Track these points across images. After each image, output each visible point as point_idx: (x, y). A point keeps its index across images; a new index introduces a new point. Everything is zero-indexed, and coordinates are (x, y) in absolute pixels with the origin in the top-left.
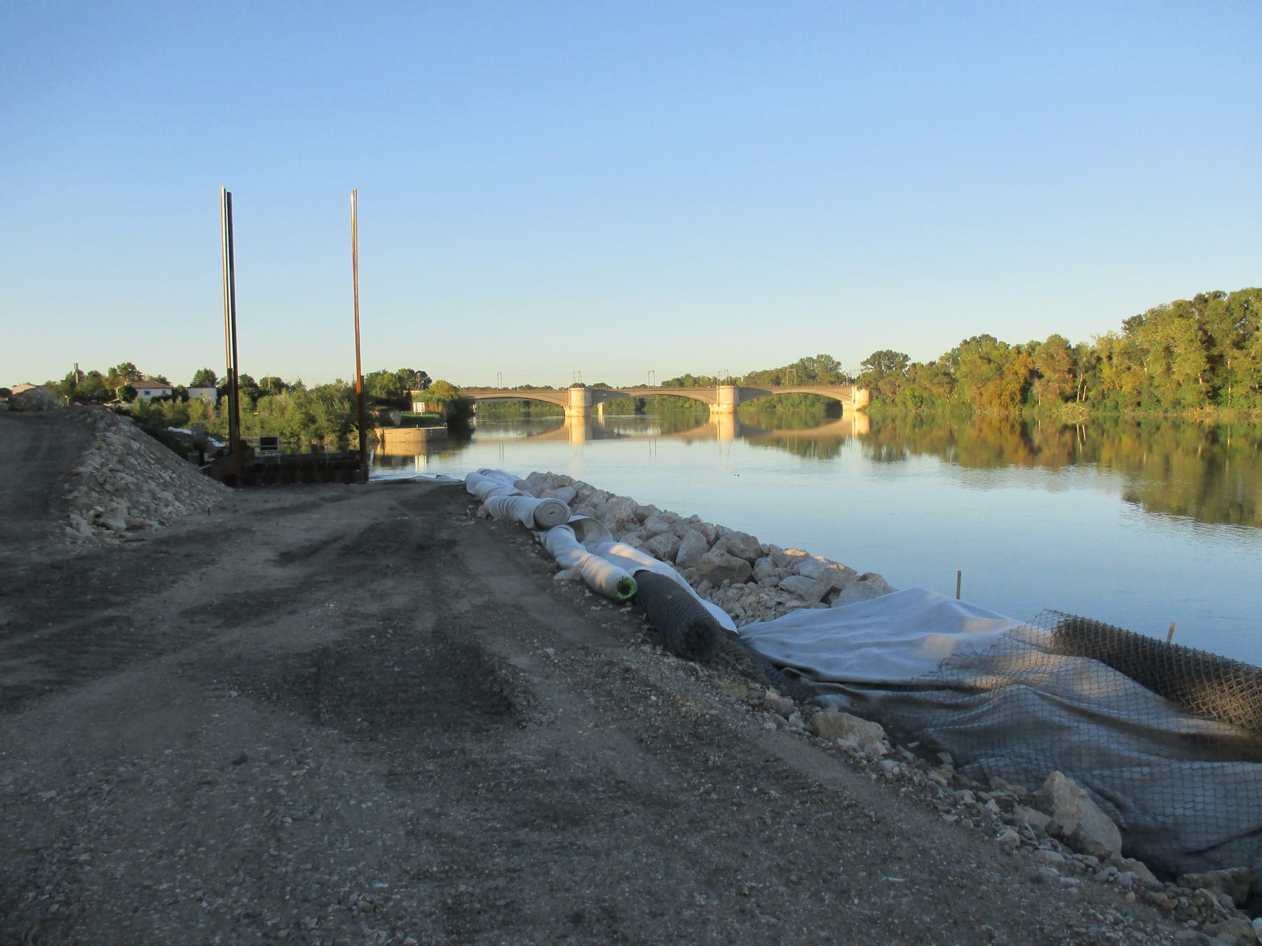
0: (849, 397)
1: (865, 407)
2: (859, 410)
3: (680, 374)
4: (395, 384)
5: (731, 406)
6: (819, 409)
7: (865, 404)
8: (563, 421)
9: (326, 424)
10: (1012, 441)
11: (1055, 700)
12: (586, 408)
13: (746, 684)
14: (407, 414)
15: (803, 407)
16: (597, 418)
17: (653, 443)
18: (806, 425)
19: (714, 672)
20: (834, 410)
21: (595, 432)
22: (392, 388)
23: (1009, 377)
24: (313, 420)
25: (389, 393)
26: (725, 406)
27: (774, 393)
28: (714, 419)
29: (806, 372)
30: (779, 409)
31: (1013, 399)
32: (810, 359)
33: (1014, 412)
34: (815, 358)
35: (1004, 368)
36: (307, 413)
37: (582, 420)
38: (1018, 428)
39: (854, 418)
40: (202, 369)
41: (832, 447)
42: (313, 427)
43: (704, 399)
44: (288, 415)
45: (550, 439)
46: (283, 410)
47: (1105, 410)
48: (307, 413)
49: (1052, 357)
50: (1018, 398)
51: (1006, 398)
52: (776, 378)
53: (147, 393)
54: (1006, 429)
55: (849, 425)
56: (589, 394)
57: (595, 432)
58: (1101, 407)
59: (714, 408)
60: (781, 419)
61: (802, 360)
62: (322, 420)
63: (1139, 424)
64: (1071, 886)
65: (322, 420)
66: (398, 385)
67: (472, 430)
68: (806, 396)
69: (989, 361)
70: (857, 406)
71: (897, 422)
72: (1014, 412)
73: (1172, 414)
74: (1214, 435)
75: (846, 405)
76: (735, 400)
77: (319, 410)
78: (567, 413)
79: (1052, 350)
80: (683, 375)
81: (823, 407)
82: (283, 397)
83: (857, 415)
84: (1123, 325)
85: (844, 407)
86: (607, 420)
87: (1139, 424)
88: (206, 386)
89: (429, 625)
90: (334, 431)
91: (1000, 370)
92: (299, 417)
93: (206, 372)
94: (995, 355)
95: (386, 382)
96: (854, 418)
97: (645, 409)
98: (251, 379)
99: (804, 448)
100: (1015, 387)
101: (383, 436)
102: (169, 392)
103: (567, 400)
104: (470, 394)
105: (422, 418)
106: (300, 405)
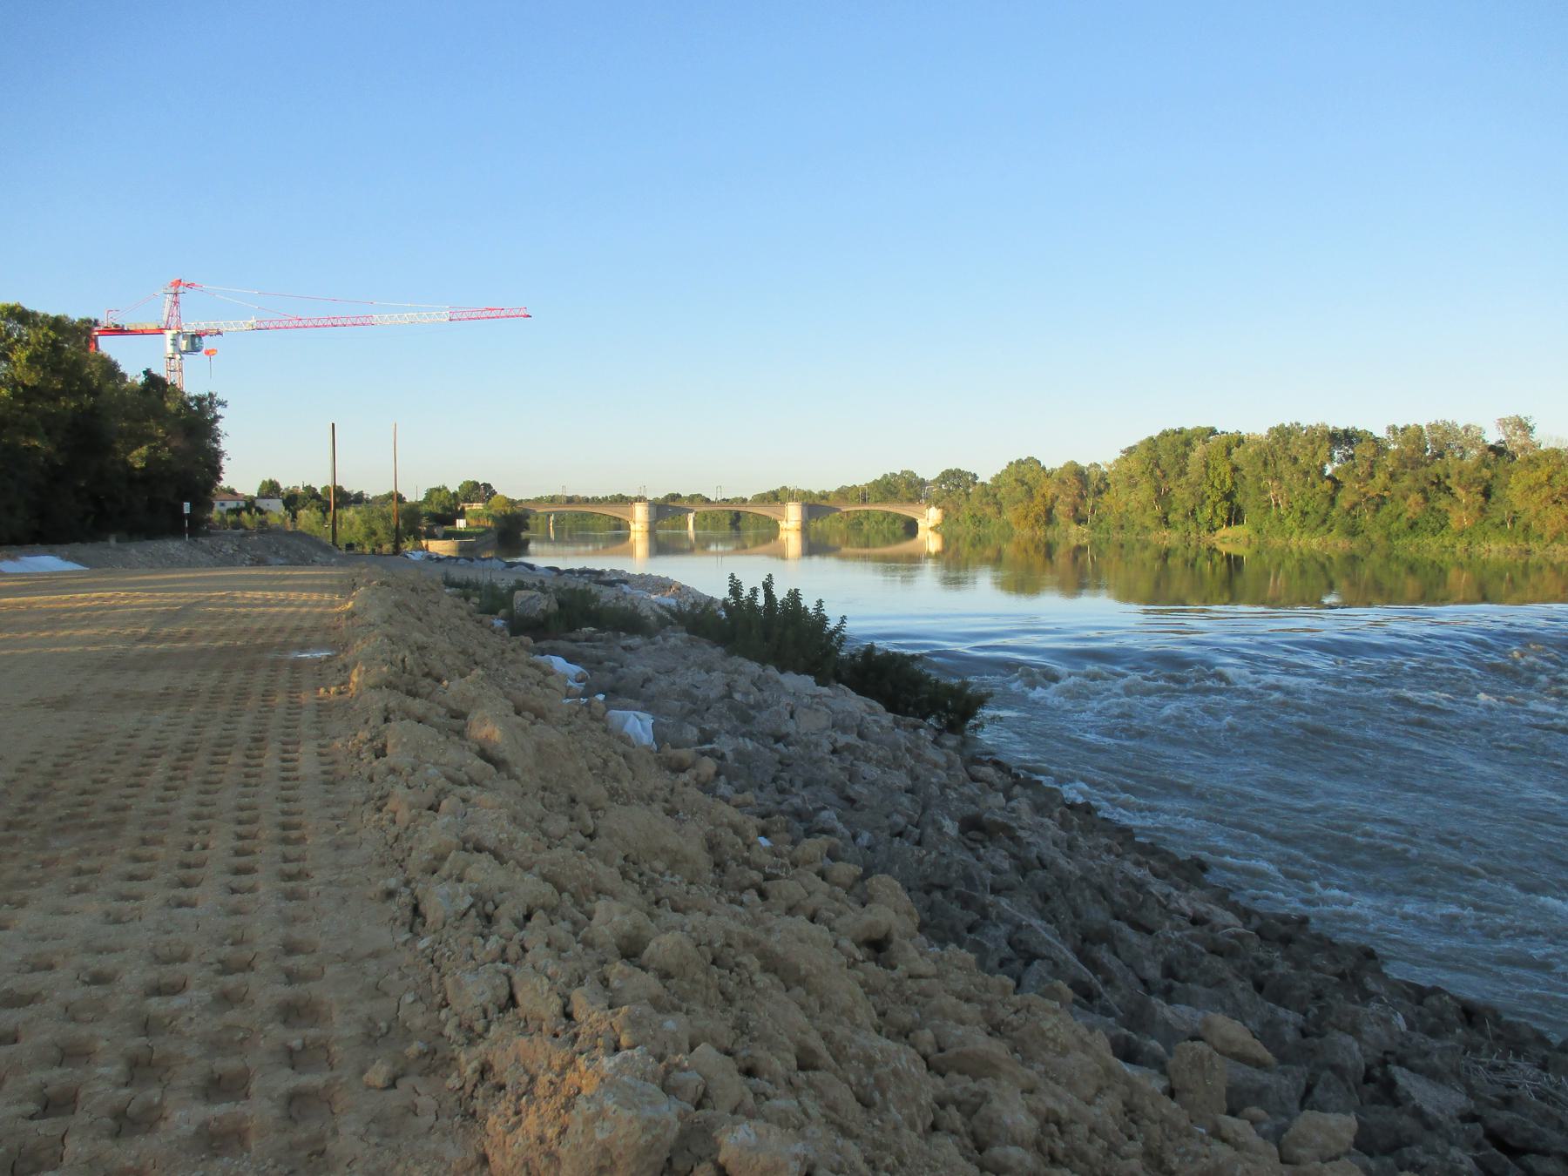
0: (923, 515)
1: (937, 526)
2: (931, 529)
3: (775, 487)
4: (449, 500)
5: (799, 523)
6: (899, 525)
8: (629, 535)
9: (384, 536)
12: (650, 523)
14: (449, 528)
15: (885, 525)
16: (687, 535)
17: (720, 559)
18: (887, 542)
19: (744, 730)
21: (814, 546)
22: (447, 504)
24: (374, 533)
25: (444, 508)
26: (793, 523)
27: (845, 509)
28: (783, 535)
31: (1037, 521)
32: (894, 475)
34: (899, 473)
36: (370, 528)
37: (646, 535)
39: (929, 540)
40: (267, 480)
42: (374, 538)
43: (773, 516)
44: (355, 529)
45: (612, 554)
46: (351, 524)
47: (1100, 533)
48: (370, 528)
49: (1064, 483)
51: (1031, 520)
53: (222, 505)
55: (923, 543)
56: (654, 509)
57: (814, 546)
59: (783, 525)
61: (885, 476)
62: (381, 533)
63: (1122, 546)
65: (381, 533)
66: (453, 501)
67: (527, 542)
68: (888, 514)
70: (931, 524)
71: (960, 542)
73: (1118, 536)
74: (1165, 555)
75: (921, 524)
77: (379, 526)
78: (632, 527)
80: (778, 487)
82: (349, 513)
83: (930, 534)
85: (920, 525)
86: (696, 536)
88: (272, 498)
89: (133, 551)
90: (390, 542)
92: (363, 530)
93: (271, 482)
95: (442, 498)
97: (740, 524)
98: (315, 489)
101: (427, 546)
102: (242, 504)
103: (632, 514)
104: (525, 506)
105: (464, 533)
106: (365, 522)
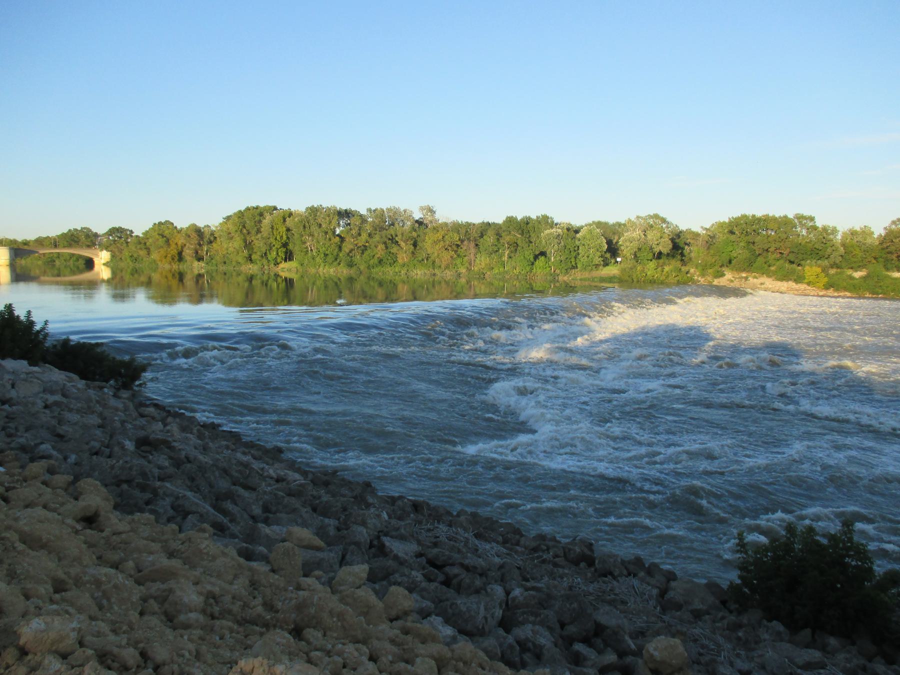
0: (97, 255)
1: (108, 262)
2: (104, 264)
6: (81, 263)
7: (109, 260)
10: (174, 283)
11: (330, 356)
13: (491, 338)
18: (73, 273)
20: (89, 264)
23: (173, 246)
27: (41, 252)
29: (73, 238)
30: (57, 263)
31: (173, 259)
33: (175, 267)
35: (170, 242)
38: (177, 276)
41: (93, 285)
49: (189, 236)
50: (177, 258)
52: (55, 242)
54: (170, 276)
58: (210, 264)
60: (59, 269)
64: (78, 411)
68: (73, 255)
69: (163, 236)
70: (103, 261)
72: (175, 267)
73: (222, 268)
74: (251, 279)
76: (11, 256)
79: (189, 233)
81: (84, 262)
83: (103, 267)
84: (863, 227)
87: (225, 274)
91: (168, 241)
94: (166, 233)
96: (103, 271)
99: (75, 286)
100: (175, 252)
